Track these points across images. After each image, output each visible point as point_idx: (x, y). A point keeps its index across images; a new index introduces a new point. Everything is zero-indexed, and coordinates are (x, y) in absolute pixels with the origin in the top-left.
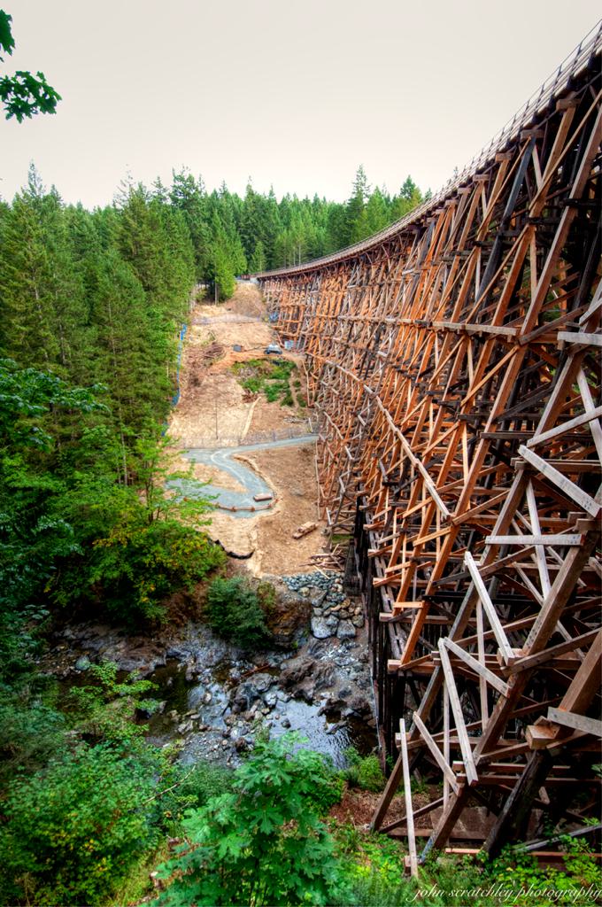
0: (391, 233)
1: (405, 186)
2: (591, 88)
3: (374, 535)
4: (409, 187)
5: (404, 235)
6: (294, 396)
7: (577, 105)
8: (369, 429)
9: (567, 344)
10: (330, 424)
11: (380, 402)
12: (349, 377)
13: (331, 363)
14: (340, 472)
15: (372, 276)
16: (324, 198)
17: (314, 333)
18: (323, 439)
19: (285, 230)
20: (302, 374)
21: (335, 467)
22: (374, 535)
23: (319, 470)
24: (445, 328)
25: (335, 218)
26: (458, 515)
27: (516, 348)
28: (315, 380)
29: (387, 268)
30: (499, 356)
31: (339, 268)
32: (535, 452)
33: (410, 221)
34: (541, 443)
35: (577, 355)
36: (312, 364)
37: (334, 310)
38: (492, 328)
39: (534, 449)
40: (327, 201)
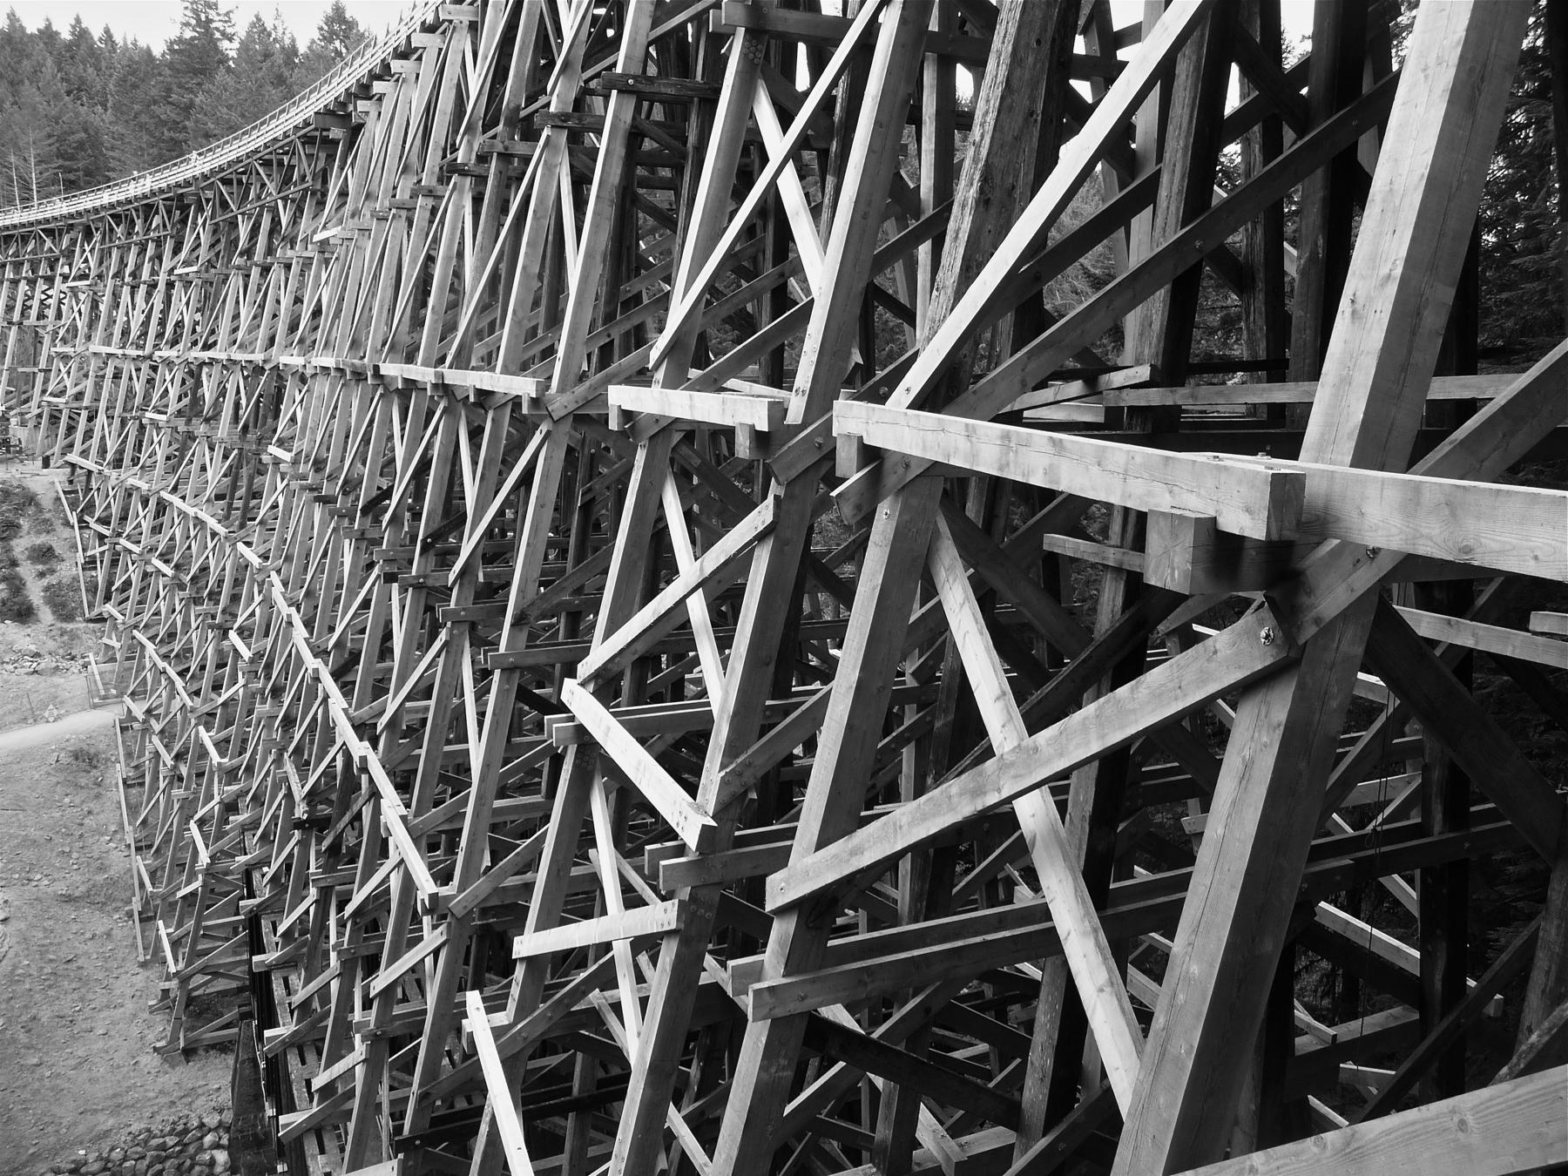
0: (279, 133)
1: (330, 21)
3: (286, 981)
4: (340, 26)
5: (308, 140)
6: (35, 592)
9: (627, 415)
11: (277, 590)
12: (199, 523)
13: (144, 486)
14: (188, 807)
15: (243, 242)
16: (107, 31)
18: (139, 710)
20: (58, 524)
21: (178, 792)
22: (286, 981)
23: (133, 809)
24: (406, 380)
25: (135, 86)
26: (461, 889)
27: (544, 428)
28: (102, 537)
29: (276, 222)
30: (516, 447)
31: (147, 219)
33: (320, 106)
36: (88, 489)
38: (500, 382)
39: (591, 687)
40: (118, 38)
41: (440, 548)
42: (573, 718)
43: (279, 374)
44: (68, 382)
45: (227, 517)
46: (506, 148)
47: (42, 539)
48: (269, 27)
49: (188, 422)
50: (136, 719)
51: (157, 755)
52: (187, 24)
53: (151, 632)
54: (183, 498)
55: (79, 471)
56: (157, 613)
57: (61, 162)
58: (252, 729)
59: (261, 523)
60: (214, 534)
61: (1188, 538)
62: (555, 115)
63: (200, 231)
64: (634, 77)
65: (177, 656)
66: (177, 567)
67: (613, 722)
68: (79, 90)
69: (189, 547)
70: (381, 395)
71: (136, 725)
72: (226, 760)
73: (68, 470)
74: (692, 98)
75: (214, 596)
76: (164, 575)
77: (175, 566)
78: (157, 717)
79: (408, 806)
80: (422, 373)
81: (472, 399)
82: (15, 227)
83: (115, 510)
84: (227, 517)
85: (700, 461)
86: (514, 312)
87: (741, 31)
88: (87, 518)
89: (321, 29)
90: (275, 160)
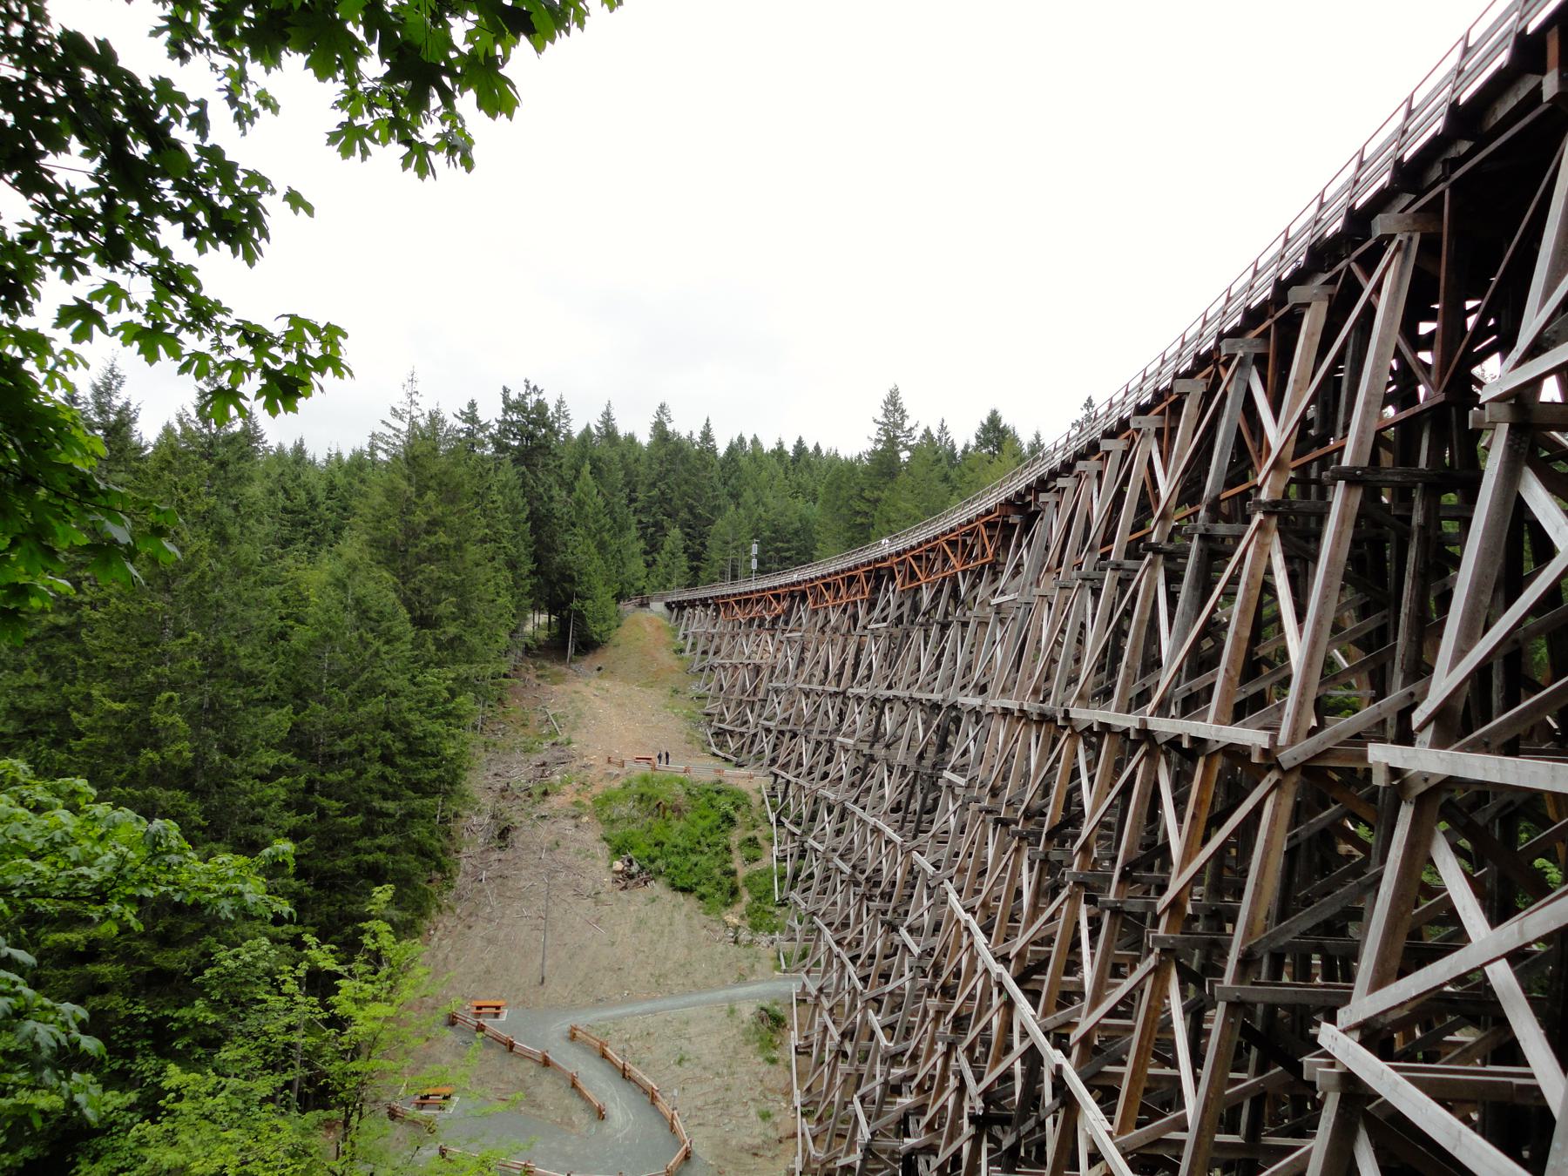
1: (985, 429)
2: (1354, 266)
7: (1330, 296)
9: (1395, 772)
13: (832, 797)
19: (733, 507)
21: (843, 1067)
32: (1361, 1042)
37: (840, 675)
38: (1210, 728)
45: (901, 828)
46: (1207, 530)
47: (751, 834)
49: (872, 746)
50: (809, 994)
51: (826, 1028)
52: (879, 441)
53: (828, 920)
54: (864, 808)
55: (780, 780)
56: (834, 904)
59: (933, 836)
60: (888, 842)
62: (1265, 504)
63: (891, 595)
64: (1362, 469)
65: (849, 944)
66: (854, 867)
70: (1069, 735)
71: (809, 999)
72: (891, 1044)
73: (772, 778)
74: (1417, 482)
75: (886, 896)
76: (842, 873)
78: (828, 995)
79: (1111, 1122)
82: (752, 592)
83: (805, 813)
84: (901, 828)
87: (1504, 428)
88: (783, 819)
90: (960, 542)
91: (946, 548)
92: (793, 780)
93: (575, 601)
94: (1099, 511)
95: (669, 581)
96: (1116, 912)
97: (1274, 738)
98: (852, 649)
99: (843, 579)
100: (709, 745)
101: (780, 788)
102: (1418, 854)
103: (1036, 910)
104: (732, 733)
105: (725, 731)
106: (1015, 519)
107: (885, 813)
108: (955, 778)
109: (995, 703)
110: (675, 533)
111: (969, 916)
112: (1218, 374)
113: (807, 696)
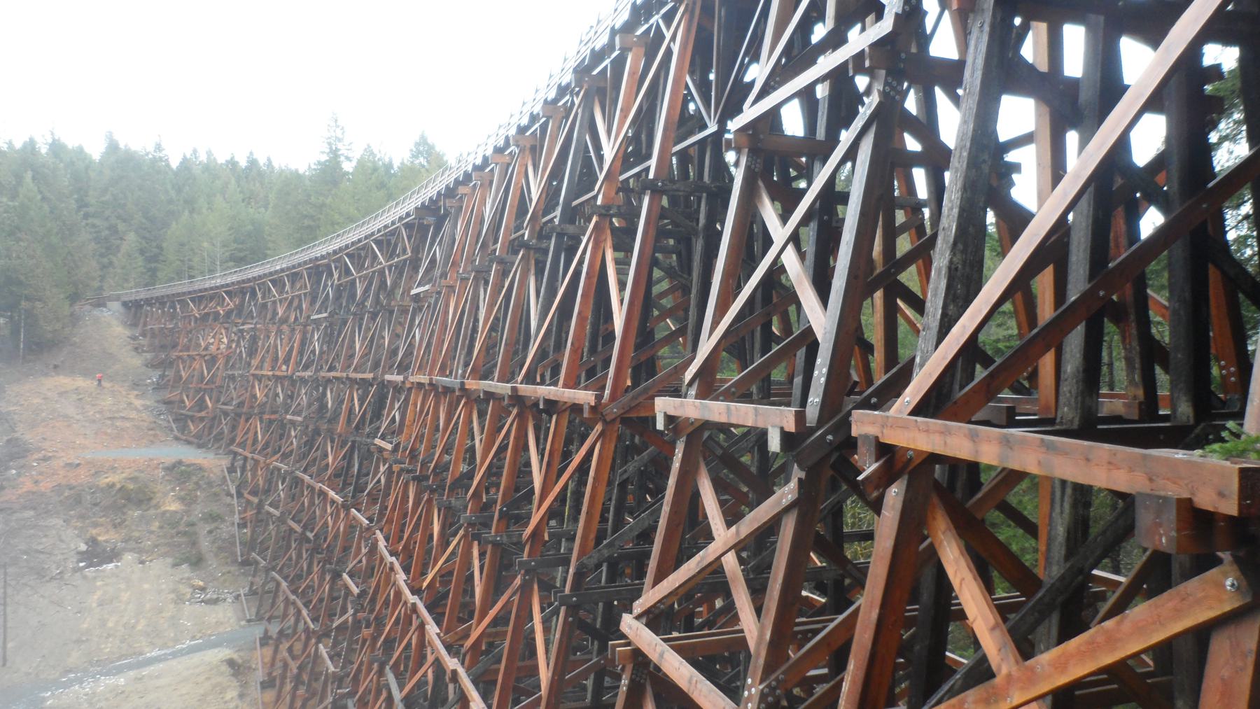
1: (417, 145)
5: (408, 226)
7: (646, 44)
8: (366, 600)
9: (670, 419)
10: (287, 599)
11: (382, 544)
16: (269, 160)
17: (245, 410)
19: (186, 213)
27: (599, 428)
32: (647, 625)
34: (654, 606)
35: (690, 437)
39: (644, 620)
41: (515, 513)
42: (629, 644)
43: (383, 385)
44: (234, 394)
48: (376, 151)
54: (311, 476)
57: (235, 245)
58: (358, 647)
60: (333, 502)
61: (1171, 515)
67: (665, 646)
68: (250, 198)
69: (314, 512)
77: (304, 526)
80: (495, 386)
81: (541, 407)
82: (206, 290)
85: (721, 452)
86: (572, 344)
89: (411, 150)
91: (374, 246)
92: (250, 455)
93: (23, 303)
94: (488, 213)
95: (127, 280)
96: (496, 545)
97: (599, 397)
98: (298, 337)
99: (287, 276)
100: (172, 430)
101: (239, 463)
102: (688, 477)
103: (445, 543)
104: (192, 418)
105: (187, 416)
106: (430, 220)
107: (329, 478)
108: (383, 444)
109: (412, 379)
110: (131, 237)
111: (393, 559)
112: (573, 101)
113: (260, 381)
